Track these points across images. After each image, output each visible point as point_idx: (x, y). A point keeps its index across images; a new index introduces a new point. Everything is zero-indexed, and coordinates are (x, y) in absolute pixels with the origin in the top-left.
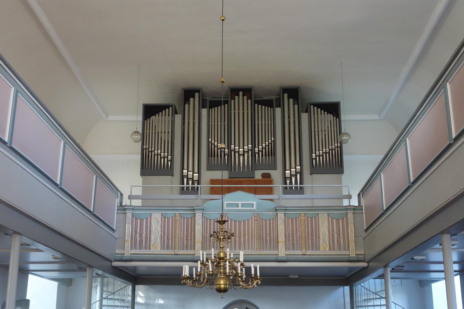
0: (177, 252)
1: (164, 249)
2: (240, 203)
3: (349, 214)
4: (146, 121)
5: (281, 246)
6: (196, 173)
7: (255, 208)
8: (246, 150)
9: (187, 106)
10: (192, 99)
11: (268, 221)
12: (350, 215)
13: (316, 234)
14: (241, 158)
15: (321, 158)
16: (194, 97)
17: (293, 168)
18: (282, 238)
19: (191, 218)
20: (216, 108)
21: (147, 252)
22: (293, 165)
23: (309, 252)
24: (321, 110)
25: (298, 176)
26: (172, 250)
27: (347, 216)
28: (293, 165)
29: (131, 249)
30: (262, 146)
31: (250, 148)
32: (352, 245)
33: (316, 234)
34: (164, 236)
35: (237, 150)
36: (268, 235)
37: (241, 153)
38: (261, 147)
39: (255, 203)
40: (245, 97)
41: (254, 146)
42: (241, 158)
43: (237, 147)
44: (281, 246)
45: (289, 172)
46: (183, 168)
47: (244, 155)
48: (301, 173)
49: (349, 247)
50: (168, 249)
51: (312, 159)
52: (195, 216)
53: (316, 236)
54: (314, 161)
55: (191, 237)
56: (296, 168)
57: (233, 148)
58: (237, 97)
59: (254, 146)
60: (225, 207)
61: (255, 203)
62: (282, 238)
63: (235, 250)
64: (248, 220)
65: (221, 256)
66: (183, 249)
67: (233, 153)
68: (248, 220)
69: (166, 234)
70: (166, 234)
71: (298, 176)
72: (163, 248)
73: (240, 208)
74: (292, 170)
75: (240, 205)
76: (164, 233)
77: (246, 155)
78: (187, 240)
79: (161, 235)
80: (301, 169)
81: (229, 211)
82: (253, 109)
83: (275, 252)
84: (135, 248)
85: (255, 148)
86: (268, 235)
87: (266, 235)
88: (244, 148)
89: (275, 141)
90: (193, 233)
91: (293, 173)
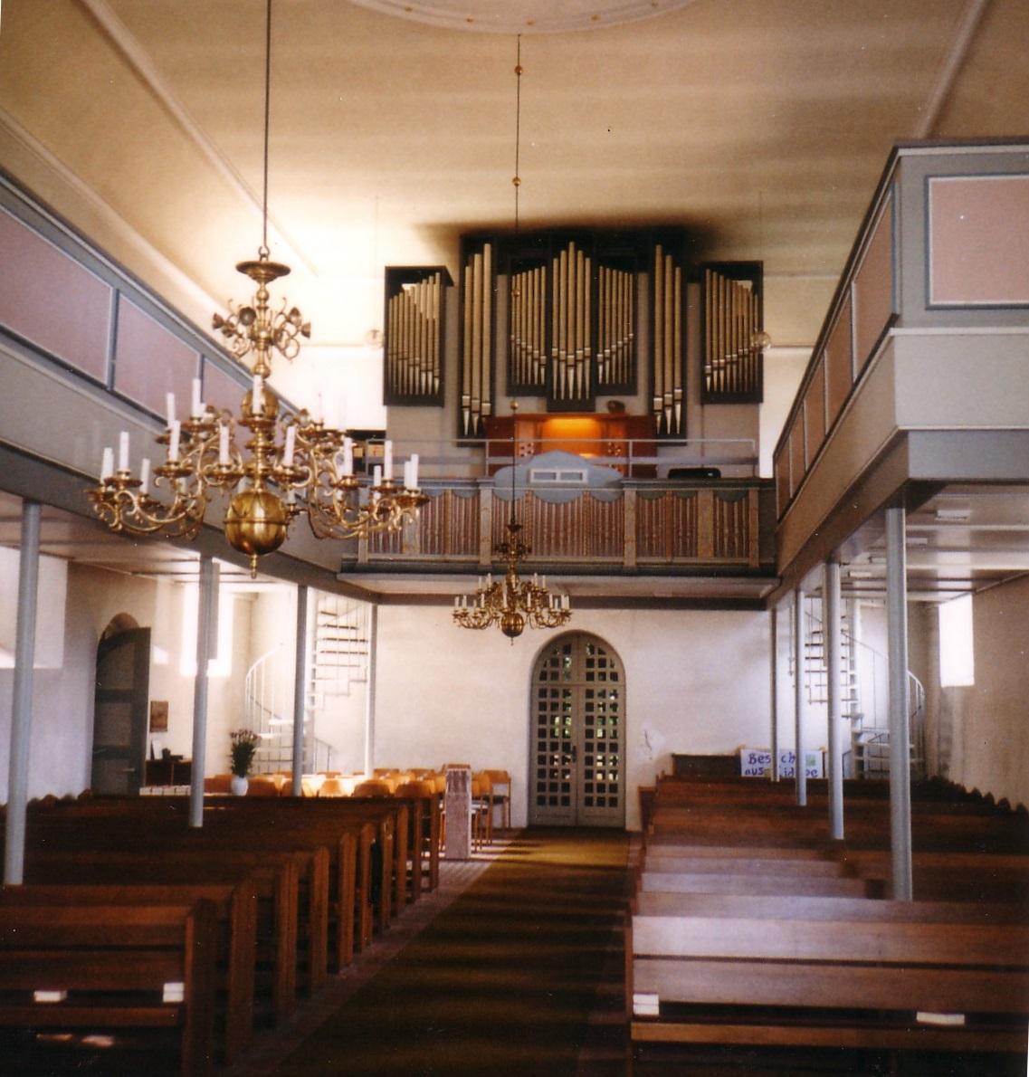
0: (448, 557)
1: (426, 552)
2: (558, 472)
3: (750, 494)
4: (391, 301)
5: (630, 547)
6: (486, 402)
7: (585, 480)
8: (580, 357)
9: (468, 269)
10: (477, 257)
11: (607, 505)
12: (753, 495)
13: (691, 528)
14: (571, 372)
15: (734, 367)
16: (482, 252)
17: (668, 393)
18: (630, 534)
19: (473, 499)
20: (524, 274)
21: (398, 556)
22: (668, 388)
23: (678, 560)
24: (725, 279)
25: (678, 407)
26: (439, 553)
27: (747, 493)
28: (668, 388)
29: (370, 551)
30: (611, 349)
31: (588, 354)
32: (755, 547)
33: (691, 528)
34: (426, 529)
35: (563, 358)
36: (607, 528)
37: (571, 362)
38: (620, 343)
39: (585, 472)
40: (580, 253)
41: (595, 350)
42: (571, 372)
43: (563, 353)
44: (630, 547)
45: (670, 396)
46: (461, 393)
47: (575, 366)
48: (684, 401)
49: (748, 551)
50: (432, 552)
51: (703, 375)
52: (478, 493)
53: (691, 532)
54: (709, 379)
55: (473, 531)
56: (673, 393)
57: (555, 354)
58: (563, 253)
59: (595, 350)
60: (533, 480)
61: (585, 472)
62: (630, 534)
63: (536, 555)
64: (573, 503)
65: (252, 531)
66: (459, 553)
67: (555, 363)
68: (573, 503)
69: (430, 526)
70: (430, 526)
71: (678, 407)
72: (424, 550)
73: (558, 480)
74: (666, 396)
75: (558, 475)
76: (426, 525)
77: (580, 365)
78: (125, 685)
79: (421, 528)
80: (684, 394)
81: (537, 486)
82: (594, 274)
83: (618, 559)
84: (376, 551)
85: (597, 352)
86: (607, 528)
87: (603, 529)
88: (575, 354)
89: (635, 340)
90: (476, 524)
91: (668, 402)
